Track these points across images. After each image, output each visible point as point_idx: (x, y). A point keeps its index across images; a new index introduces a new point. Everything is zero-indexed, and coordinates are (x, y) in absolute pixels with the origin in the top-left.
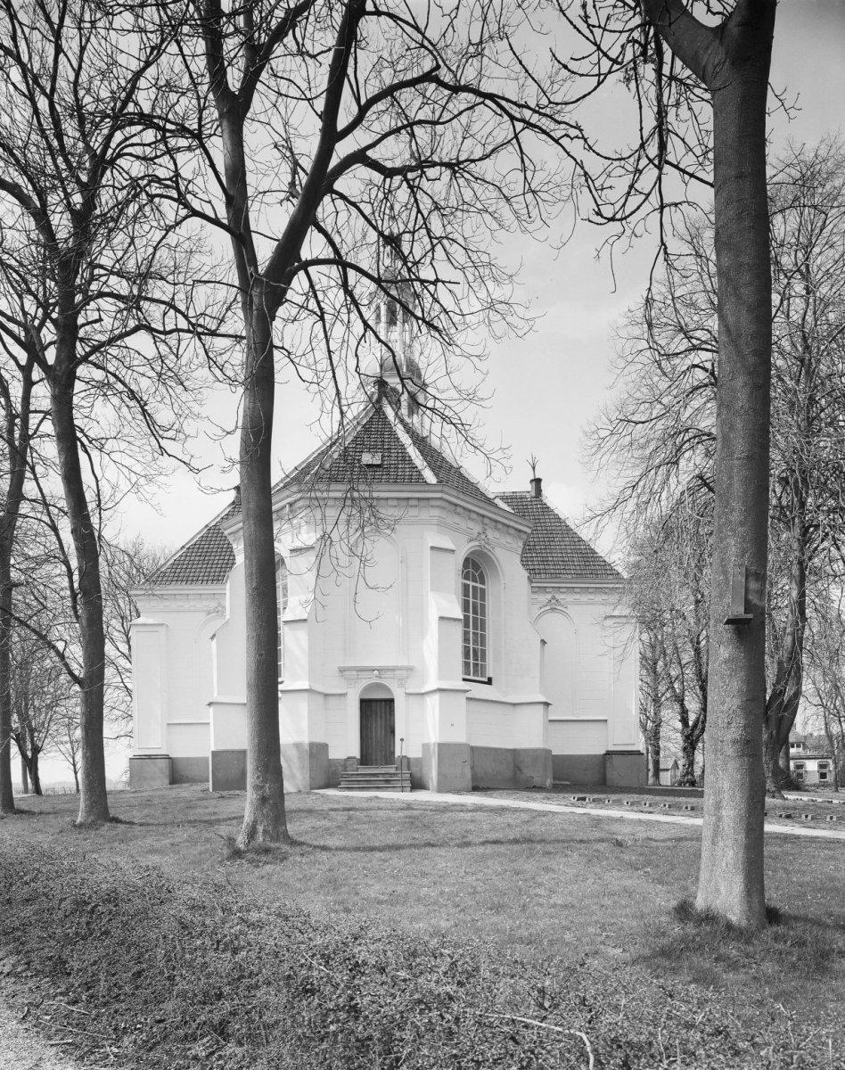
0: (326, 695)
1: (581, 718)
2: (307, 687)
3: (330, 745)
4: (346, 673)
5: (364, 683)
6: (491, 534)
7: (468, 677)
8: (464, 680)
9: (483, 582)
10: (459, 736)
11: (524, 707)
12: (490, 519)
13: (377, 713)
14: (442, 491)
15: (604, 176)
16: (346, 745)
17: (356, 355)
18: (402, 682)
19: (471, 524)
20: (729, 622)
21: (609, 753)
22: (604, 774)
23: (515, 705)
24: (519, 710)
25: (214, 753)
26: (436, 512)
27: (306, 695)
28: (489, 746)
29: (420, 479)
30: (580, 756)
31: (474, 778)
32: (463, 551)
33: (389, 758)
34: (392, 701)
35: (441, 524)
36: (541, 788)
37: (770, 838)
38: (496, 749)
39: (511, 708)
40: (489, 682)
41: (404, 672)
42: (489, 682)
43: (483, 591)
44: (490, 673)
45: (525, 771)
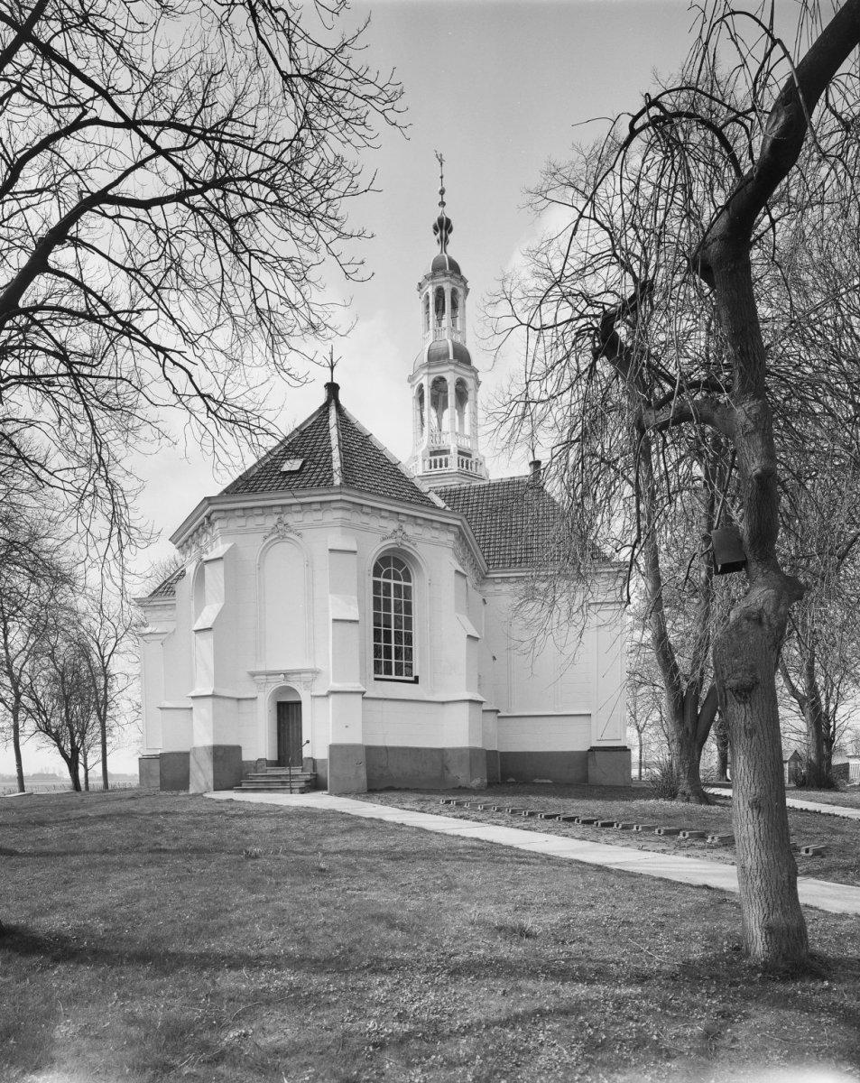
0: (239, 700)
1: (526, 714)
2: (210, 693)
3: (331, 742)
4: (256, 677)
5: (273, 687)
6: (410, 530)
7: (378, 676)
8: (376, 679)
9: (408, 579)
10: (355, 737)
11: (450, 705)
12: (368, 506)
13: (287, 712)
14: (341, 493)
15: (302, 35)
16: (259, 744)
17: (167, 379)
18: (308, 685)
19: (383, 523)
20: (483, 579)
21: (593, 749)
22: (587, 772)
23: (443, 703)
24: (447, 707)
25: (333, 748)
26: (339, 514)
27: (210, 701)
28: (406, 745)
29: (440, 494)
30: (564, 753)
31: (369, 780)
32: (373, 549)
33: (299, 760)
34: (299, 703)
35: (346, 526)
36: (465, 788)
37: (846, 869)
38: (418, 750)
39: (440, 706)
40: (416, 681)
41: (310, 675)
42: (416, 681)
43: (408, 589)
44: (416, 672)
45: (452, 772)
